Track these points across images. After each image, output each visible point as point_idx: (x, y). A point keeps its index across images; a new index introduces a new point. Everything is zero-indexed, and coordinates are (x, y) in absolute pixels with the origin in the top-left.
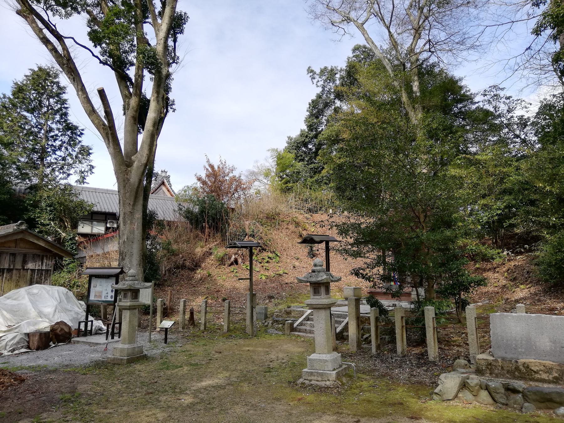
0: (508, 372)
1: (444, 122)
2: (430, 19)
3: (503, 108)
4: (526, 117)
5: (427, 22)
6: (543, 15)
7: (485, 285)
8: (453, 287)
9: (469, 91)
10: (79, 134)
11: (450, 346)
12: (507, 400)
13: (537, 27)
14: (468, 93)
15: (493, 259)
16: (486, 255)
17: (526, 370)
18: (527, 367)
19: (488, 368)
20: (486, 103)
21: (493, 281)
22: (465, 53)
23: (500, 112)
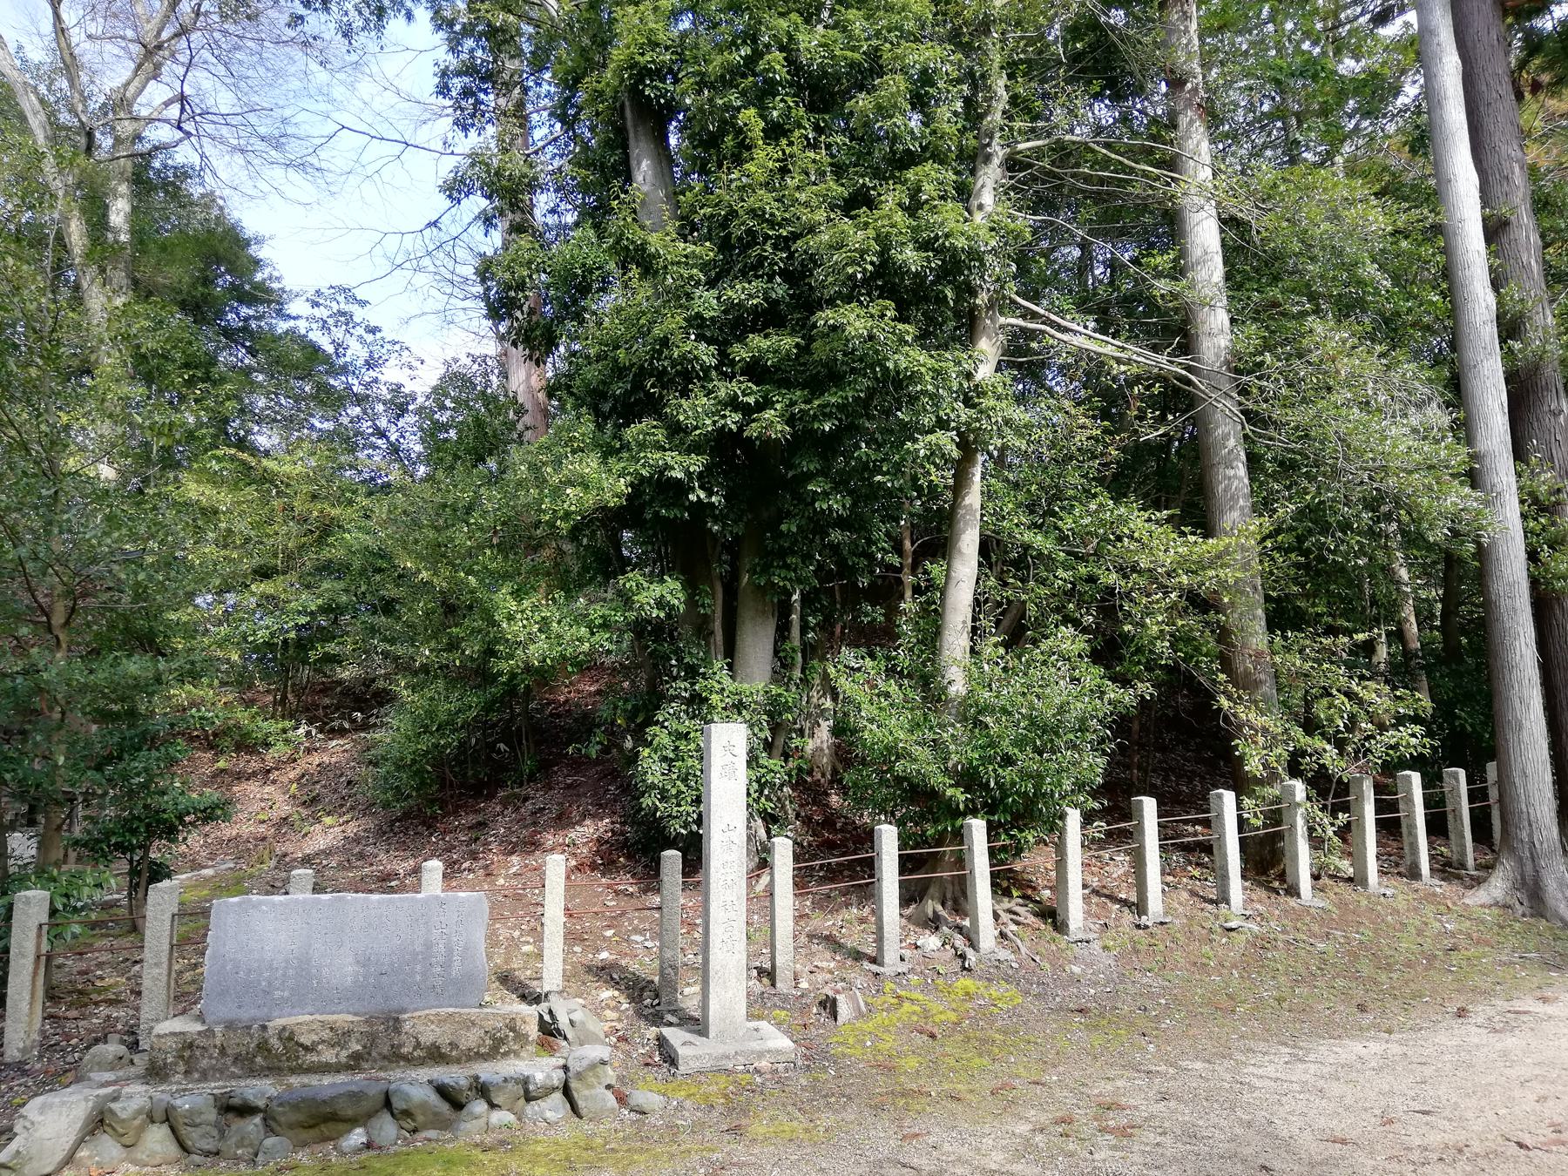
0: (237, 1059)
1: (190, 343)
2: (193, 37)
3: (356, 352)
4: (406, 390)
5: (183, 43)
6: (469, 156)
7: (227, 818)
8: (128, 826)
9: (278, 279)
10: (1077, 253)
11: (86, 1005)
12: (219, 1140)
13: (455, 180)
14: (275, 286)
15: (267, 745)
16: (248, 735)
17: (285, 1048)
18: (287, 1036)
19: (182, 1057)
20: (314, 326)
21: (256, 807)
22: (277, 173)
23: (348, 359)
